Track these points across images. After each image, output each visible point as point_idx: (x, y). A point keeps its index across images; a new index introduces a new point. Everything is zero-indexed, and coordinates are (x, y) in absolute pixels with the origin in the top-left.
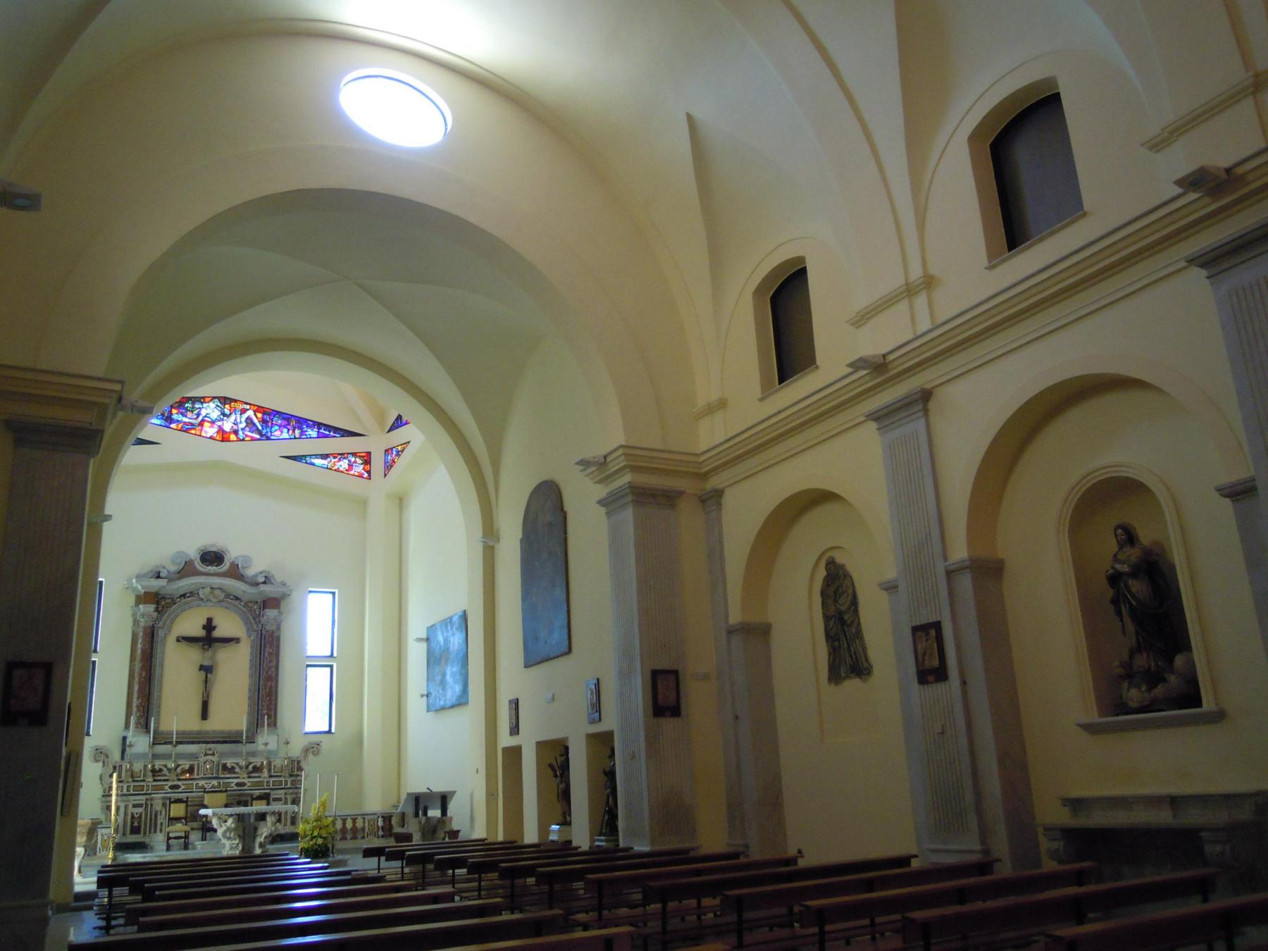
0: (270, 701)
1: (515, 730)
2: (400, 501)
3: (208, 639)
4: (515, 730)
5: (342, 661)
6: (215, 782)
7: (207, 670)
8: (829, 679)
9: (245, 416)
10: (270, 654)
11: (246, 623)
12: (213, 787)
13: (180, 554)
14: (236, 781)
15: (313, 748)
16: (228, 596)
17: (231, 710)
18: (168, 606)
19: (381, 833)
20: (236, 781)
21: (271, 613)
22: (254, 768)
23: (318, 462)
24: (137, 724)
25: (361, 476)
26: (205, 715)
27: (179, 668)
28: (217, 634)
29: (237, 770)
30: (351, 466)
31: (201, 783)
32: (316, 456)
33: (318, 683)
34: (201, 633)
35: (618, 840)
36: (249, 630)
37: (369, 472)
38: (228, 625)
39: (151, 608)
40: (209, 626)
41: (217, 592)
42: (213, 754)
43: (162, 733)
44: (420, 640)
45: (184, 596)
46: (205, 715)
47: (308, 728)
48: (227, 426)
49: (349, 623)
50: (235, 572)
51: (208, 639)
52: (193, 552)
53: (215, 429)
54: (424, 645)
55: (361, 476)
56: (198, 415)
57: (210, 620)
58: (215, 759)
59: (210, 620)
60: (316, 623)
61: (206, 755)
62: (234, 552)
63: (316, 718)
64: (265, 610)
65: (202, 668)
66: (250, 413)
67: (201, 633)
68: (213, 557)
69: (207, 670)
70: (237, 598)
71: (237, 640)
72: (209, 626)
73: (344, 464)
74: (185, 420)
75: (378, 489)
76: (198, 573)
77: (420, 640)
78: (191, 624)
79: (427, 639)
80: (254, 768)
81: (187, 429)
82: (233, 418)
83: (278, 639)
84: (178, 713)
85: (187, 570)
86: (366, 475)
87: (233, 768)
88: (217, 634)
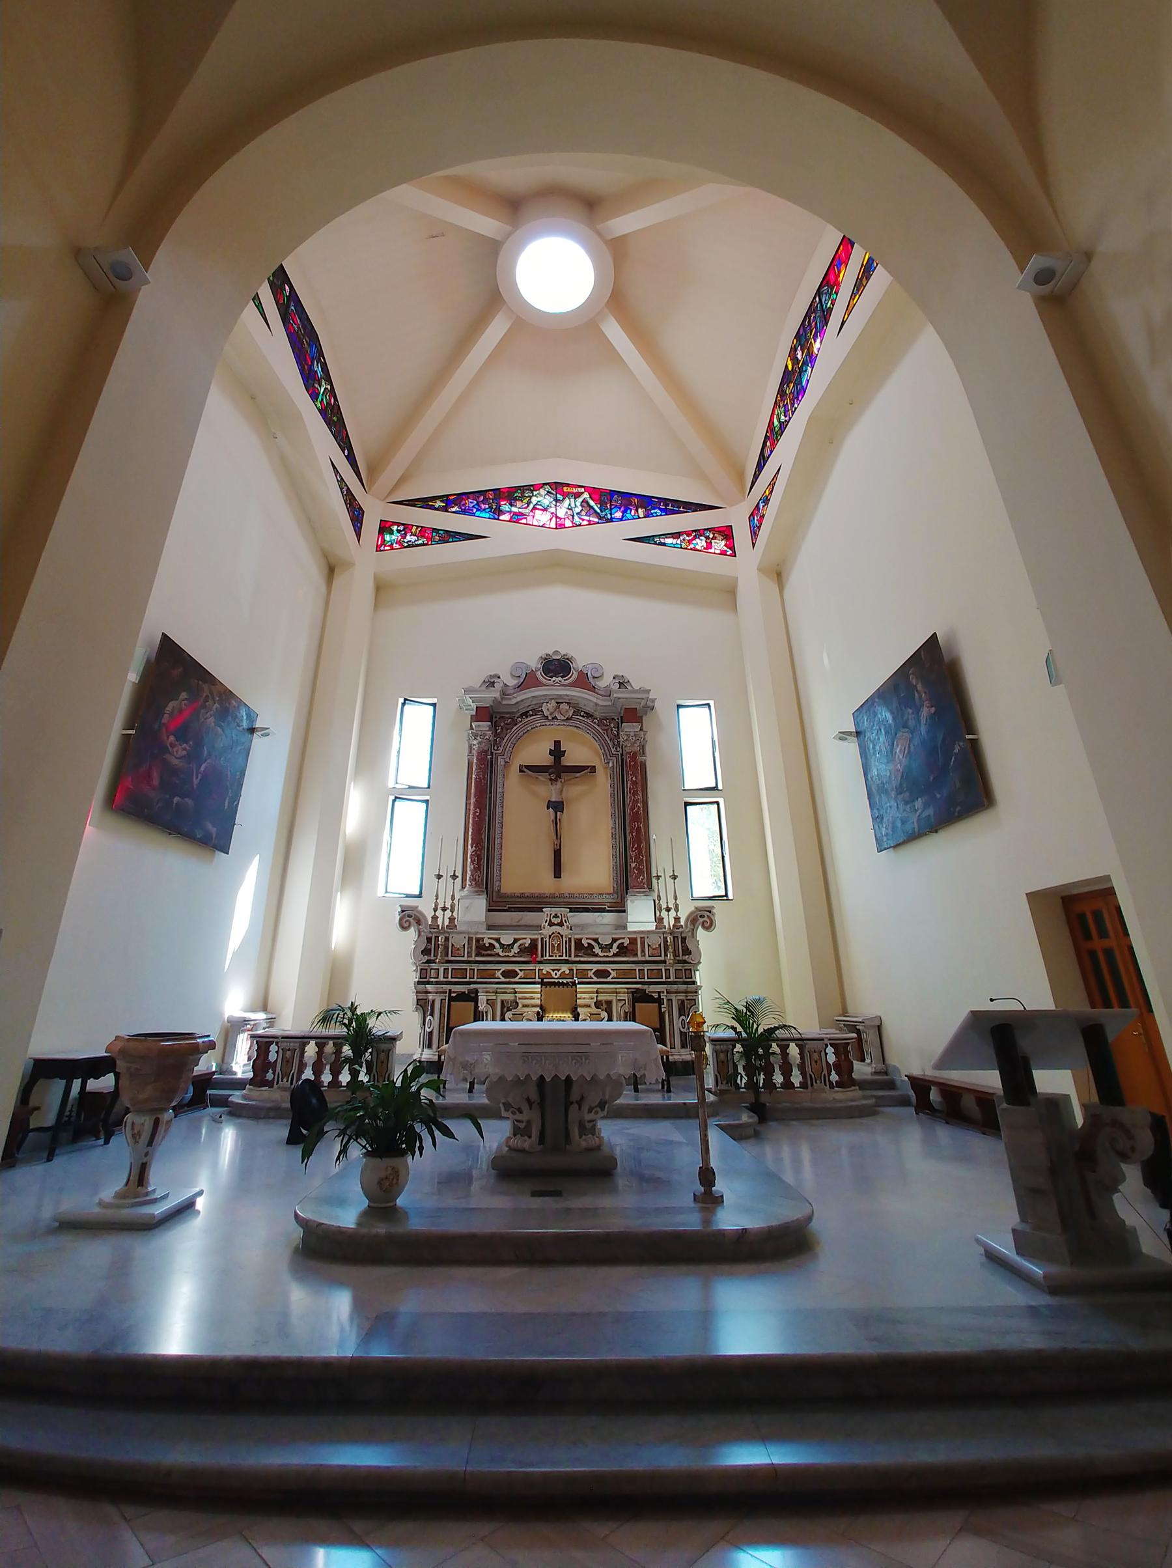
0: (639, 849)
1: (524, 1006)
2: (778, 575)
3: (558, 768)
4: (524, 1006)
5: (732, 792)
6: (565, 968)
7: (557, 806)
8: (1111, 892)
9: (580, 500)
10: (634, 783)
11: (603, 744)
12: (563, 975)
13: (518, 666)
14: (595, 967)
15: (703, 917)
16: (577, 712)
17: (593, 868)
18: (509, 726)
19: (834, 1077)
20: (595, 967)
21: (629, 728)
22: (621, 946)
23: (669, 541)
24: (473, 879)
25: (723, 553)
26: (558, 874)
27: (522, 805)
28: (567, 761)
29: (597, 950)
30: (709, 546)
31: (547, 968)
32: (666, 535)
33: (703, 824)
34: (548, 760)
35: (649, 932)
36: (608, 754)
37: (732, 548)
38: (580, 751)
39: (485, 726)
40: (557, 752)
41: (564, 706)
42: (561, 924)
43: (505, 896)
44: (843, 736)
45: (526, 714)
46: (558, 874)
47: (697, 893)
48: (562, 512)
49: (732, 746)
50: (584, 682)
51: (558, 768)
52: (534, 663)
53: (548, 516)
54: (853, 746)
55: (723, 553)
56: (529, 503)
57: (557, 744)
58: (564, 931)
59: (557, 744)
60: (694, 744)
61: (551, 924)
62: (581, 661)
63: (705, 880)
64: (624, 732)
65: (550, 804)
66: (586, 495)
67: (548, 760)
68: (557, 666)
69: (557, 806)
70: (588, 715)
71: (593, 769)
72: (557, 752)
73: (701, 543)
74: (514, 509)
75: (746, 564)
76: (539, 684)
77: (843, 736)
78: (537, 752)
79: (858, 734)
80: (621, 946)
81: (517, 518)
82: (567, 502)
83: (644, 766)
84: (523, 869)
85: (528, 681)
86: (729, 552)
87: (591, 946)
88: (567, 761)
